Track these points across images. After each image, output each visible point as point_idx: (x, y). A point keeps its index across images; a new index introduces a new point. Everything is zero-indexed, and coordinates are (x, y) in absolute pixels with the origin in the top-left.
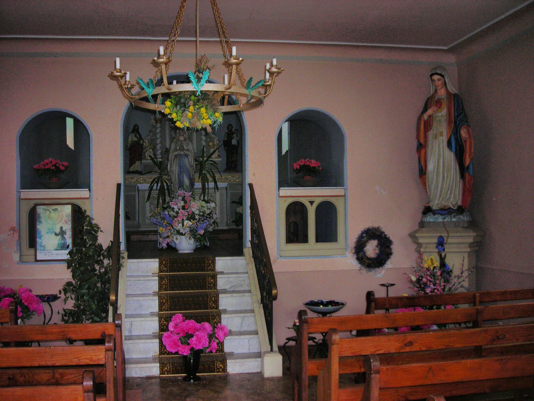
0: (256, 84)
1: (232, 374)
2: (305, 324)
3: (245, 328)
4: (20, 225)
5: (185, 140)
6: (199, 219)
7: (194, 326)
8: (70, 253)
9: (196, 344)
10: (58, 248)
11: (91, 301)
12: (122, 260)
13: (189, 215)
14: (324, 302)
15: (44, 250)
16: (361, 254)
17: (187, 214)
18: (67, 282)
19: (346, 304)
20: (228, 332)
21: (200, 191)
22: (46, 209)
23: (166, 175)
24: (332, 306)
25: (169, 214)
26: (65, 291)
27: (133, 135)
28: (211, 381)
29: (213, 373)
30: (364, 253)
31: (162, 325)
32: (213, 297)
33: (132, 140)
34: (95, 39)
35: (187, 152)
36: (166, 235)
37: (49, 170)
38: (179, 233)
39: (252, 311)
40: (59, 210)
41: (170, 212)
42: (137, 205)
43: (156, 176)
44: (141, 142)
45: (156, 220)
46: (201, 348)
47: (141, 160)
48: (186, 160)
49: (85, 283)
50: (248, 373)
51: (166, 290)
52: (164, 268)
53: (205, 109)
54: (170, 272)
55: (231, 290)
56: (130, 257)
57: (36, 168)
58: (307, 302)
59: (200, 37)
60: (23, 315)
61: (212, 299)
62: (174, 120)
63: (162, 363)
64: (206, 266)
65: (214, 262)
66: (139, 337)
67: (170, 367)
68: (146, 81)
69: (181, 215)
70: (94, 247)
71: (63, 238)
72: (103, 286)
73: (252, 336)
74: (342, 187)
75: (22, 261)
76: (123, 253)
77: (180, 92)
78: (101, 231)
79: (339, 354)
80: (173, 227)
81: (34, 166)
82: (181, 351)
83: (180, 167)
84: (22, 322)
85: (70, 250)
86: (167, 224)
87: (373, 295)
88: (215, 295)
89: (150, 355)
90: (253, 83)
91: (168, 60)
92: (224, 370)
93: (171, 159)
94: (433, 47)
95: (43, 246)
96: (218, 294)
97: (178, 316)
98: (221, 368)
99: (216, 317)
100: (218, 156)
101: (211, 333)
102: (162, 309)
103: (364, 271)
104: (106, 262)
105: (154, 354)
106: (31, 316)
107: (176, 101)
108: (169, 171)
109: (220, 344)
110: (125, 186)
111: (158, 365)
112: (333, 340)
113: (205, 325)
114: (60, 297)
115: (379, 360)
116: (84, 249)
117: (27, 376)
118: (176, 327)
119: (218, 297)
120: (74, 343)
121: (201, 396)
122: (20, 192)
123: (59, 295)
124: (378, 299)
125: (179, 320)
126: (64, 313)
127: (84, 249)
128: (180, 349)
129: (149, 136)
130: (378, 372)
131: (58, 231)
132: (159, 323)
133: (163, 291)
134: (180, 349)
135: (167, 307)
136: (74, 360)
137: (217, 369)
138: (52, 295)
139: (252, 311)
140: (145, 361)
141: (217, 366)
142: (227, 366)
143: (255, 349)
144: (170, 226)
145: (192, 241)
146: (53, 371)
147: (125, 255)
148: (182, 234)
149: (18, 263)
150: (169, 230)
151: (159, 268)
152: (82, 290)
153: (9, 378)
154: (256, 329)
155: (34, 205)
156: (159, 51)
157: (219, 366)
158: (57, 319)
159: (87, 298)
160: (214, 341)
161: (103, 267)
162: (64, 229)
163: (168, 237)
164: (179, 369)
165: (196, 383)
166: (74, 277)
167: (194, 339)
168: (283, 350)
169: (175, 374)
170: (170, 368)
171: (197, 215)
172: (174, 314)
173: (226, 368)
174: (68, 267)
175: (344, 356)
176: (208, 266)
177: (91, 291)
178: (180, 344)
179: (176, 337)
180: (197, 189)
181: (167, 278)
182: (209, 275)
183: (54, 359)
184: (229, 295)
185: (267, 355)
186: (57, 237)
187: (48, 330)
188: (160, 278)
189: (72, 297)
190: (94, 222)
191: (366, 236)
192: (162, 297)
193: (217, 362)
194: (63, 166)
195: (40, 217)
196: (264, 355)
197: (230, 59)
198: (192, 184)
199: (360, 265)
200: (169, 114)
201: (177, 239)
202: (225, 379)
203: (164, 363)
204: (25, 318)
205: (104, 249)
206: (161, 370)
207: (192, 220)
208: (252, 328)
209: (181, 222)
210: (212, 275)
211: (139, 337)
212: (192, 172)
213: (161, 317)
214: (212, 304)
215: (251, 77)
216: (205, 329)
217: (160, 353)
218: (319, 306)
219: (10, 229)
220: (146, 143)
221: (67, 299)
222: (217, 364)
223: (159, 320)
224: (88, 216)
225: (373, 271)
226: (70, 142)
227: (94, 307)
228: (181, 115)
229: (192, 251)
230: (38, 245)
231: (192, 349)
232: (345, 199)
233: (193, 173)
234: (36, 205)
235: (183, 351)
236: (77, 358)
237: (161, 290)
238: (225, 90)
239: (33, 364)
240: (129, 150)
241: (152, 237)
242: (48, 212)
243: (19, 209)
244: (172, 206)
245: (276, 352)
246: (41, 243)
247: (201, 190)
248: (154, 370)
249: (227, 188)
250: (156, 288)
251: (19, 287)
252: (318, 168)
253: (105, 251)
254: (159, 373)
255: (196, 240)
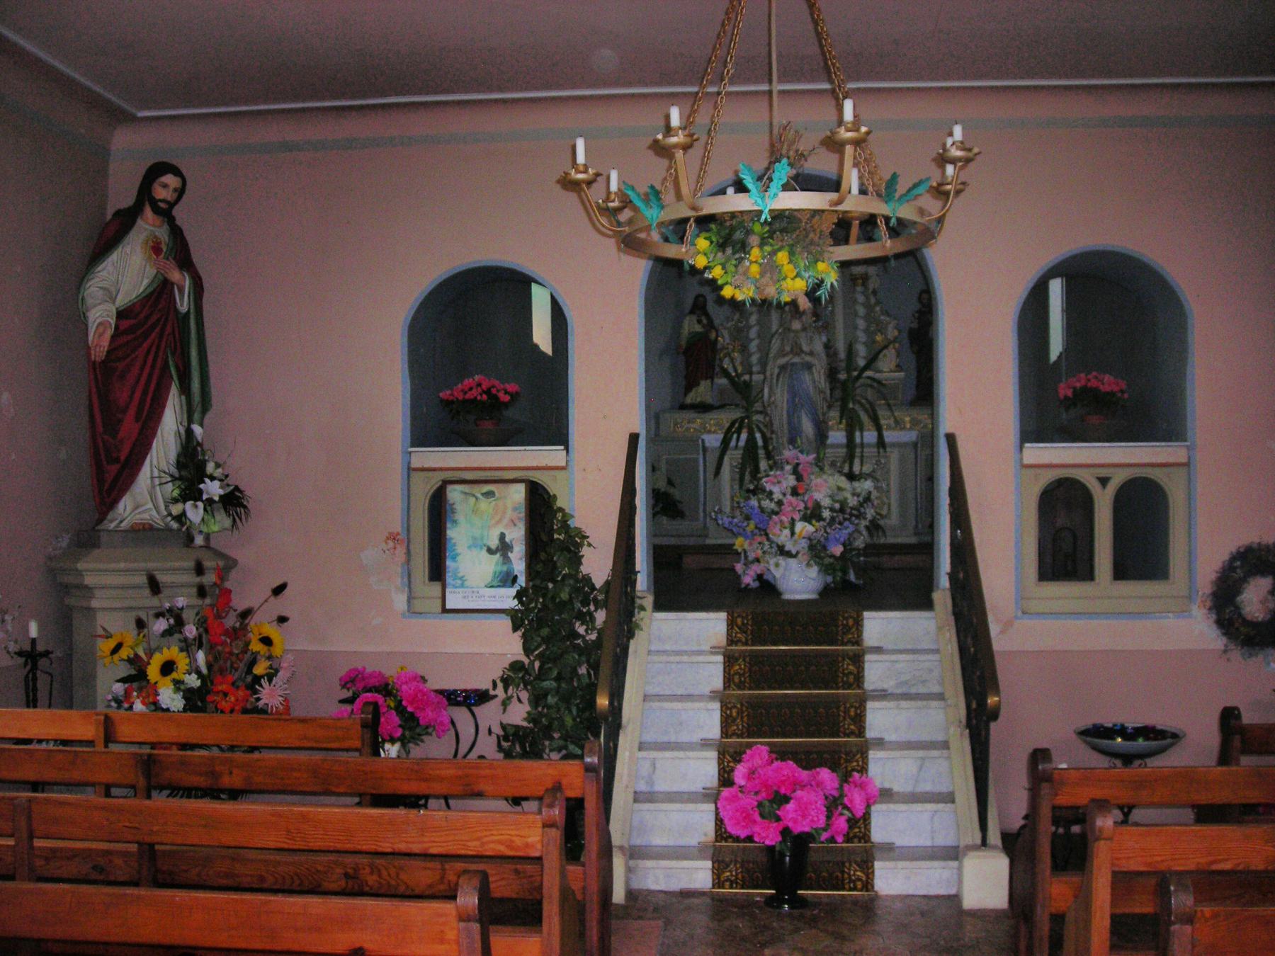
0: (910, 190)
1: (886, 896)
2: (1044, 785)
3: (927, 787)
4: (408, 530)
5: (804, 329)
6: (833, 519)
7: (794, 776)
8: (519, 596)
9: (795, 821)
10: (494, 584)
11: (562, 709)
12: (639, 613)
13: (806, 508)
14: (1127, 728)
15: (462, 586)
16: (1227, 611)
17: (802, 506)
18: (512, 661)
19: (1185, 735)
20: (877, 794)
21: (832, 451)
22: (467, 491)
23: (761, 412)
24: (1147, 738)
25: (760, 507)
26: (506, 682)
27: (694, 318)
28: (833, 910)
29: (839, 890)
30: (1237, 608)
31: (725, 771)
32: (852, 706)
33: (692, 330)
34: (884, 90)
35: (808, 358)
36: (751, 556)
37: (473, 401)
38: (782, 551)
39: (945, 745)
40: (497, 494)
41: (763, 502)
42: (702, 484)
43: (737, 414)
44: (713, 335)
45: (730, 519)
46: (807, 829)
47: (712, 379)
48: (806, 377)
49: (550, 665)
50: (925, 896)
51: (740, 686)
52: (739, 635)
53: (787, 253)
54: (752, 645)
55: (899, 691)
56: (659, 606)
57: (446, 398)
58: (1083, 729)
59: (780, 81)
60: (403, 735)
61: (849, 711)
62: (720, 282)
63: (718, 861)
64: (840, 633)
65: (858, 623)
66: (672, 797)
67: (736, 870)
68: (643, 189)
69: (787, 508)
70: (572, 582)
71: (506, 559)
72: (592, 673)
73: (941, 806)
74: (1181, 441)
75: (412, 612)
76: (640, 598)
77: (733, 215)
78: (589, 545)
79: (1113, 865)
80: (768, 539)
81: (441, 394)
82: (759, 834)
83: (793, 393)
84: (403, 751)
85: (519, 588)
86: (757, 531)
87: (1238, 717)
88: (856, 702)
89: (693, 840)
90: (901, 188)
91: (688, 140)
92: (868, 885)
93: (772, 375)
94: (1085, 82)
95: (461, 578)
96: (865, 701)
97: (761, 747)
98: (860, 880)
99: (854, 756)
100: (898, 366)
101: (835, 793)
102: (730, 733)
103: (1236, 654)
104: (600, 616)
105: (703, 839)
106: (423, 737)
107: (721, 237)
108: (766, 404)
109: (862, 821)
110: (650, 441)
111: (709, 864)
112: (1097, 828)
113: (822, 774)
114: (496, 696)
115: (1191, 889)
116: (550, 586)
117: (385, 873)
118: (750, 776)
119: (865, 707)
120: (522, 803)
121: (799, 945)
122: (410, 453)
123: (492, 693)
124: (1252, 727)
125: (761, 759)
126: (501, 733)
127: (550, 586)
128: (756, 829)
129: (733, 320)
130: (1189, 919)
131: (494, 543)
132: (719, 766)
133: (734, 690)
134: (756, 829)
135: (740, 727)
136: (469, 844)
137: (849, 883)
138: (476, 691)
139: (945, 745)
140: (679, 853)
141: (849, 874)
142: (873, 876)
143: (945, 838)
144: (761, 535)
145: (814, 572)
146: (442, 865)
147: (648, 601)
148: (789, 554)
149: (403, 615)
150: (760, 543)
151: (728, 634)
152: (544, 680)
153: (346, 875)
154: (951, 789)
155: (440, 483)
156: (667, 117)
157: (854, 875)
158: (487, 746)
159: (555, 700)
160: (841, 814)
161: (593, 628)
162: (507, 539)
163: (758, 560)
164: (757, 877)
165: (796, 912)
166: (527, 650)
167: (790, 806)
168: (1010, 843)
169: (748, 888)
170: (737, 874)
171: (825, 508)
172: (750, 745)
173: (872, 880)
174: (515, 629)
175: (1125, 870)
176: (844, 633)
177: (563, 685)
178: (759, 819)
179: (749, 801)
180: (833, 446)
181: (744, 660)
182: (845, 655)
183: (426, 839)
184: (892, 704)
185: (972, 854)
186: (492, 556)
187: (431, 772)
188: (726, 659)
189: (521, 697)
190: (573, 523)
191: (1242, 567)
192: (730, 703)
193: (850, 865)
194: (506, 392)
195: (453, 512)
196: (965, 855)
197: (838, 130)
198: (821, 435)
199: (1224, 639)
200: (706, 268)
201: (777, 565)
202: (868, 908)
203: (723, 861)
204: (409, 742)
205: (598, 586)
206: (715, 877)
207: (814, 522)
208: (944, 788)
209: (787, 525)
210: (851, 654)
211: (672, 797)
212: (821, 405)
213: (724, 752)
214: (849, 725)
215: (895, 173)
216: (820, 784)
217: (716, 836)
218: (1114, 739)
219: (388, 538)
220: (724, 339)
221: (508, 702)
222: (849, 869)
223: (719, 758)
224: (561, 510)
225: (1261, 656)
226: (542, 336)
227: (569, 721)
228: (733, 269)
229: (813, 596)
230: (448, 575)
231: (785, 832)
232: (1189, 474)
233: (825, 408)
234: (446, 483)
235: (764, 835)
236: (478, 839)
237: (729, 686)
238: (831, 206)
239: (381, 846)
240: (685, 353)
241: (716, 562)
242: (472, 500)
243: (409, 490)
244: (768, 487)
245: (994, 847)
246: (457, 569)
247: (844, 450)
248: (699, 875)
249: (915, 445)
250: (718, 683)
251: (399, 670)
252: (1119, 395)
253: (600, 591)
254: (710, 885)
255: (826, 569)
